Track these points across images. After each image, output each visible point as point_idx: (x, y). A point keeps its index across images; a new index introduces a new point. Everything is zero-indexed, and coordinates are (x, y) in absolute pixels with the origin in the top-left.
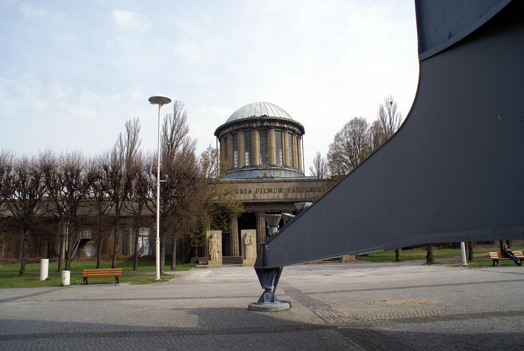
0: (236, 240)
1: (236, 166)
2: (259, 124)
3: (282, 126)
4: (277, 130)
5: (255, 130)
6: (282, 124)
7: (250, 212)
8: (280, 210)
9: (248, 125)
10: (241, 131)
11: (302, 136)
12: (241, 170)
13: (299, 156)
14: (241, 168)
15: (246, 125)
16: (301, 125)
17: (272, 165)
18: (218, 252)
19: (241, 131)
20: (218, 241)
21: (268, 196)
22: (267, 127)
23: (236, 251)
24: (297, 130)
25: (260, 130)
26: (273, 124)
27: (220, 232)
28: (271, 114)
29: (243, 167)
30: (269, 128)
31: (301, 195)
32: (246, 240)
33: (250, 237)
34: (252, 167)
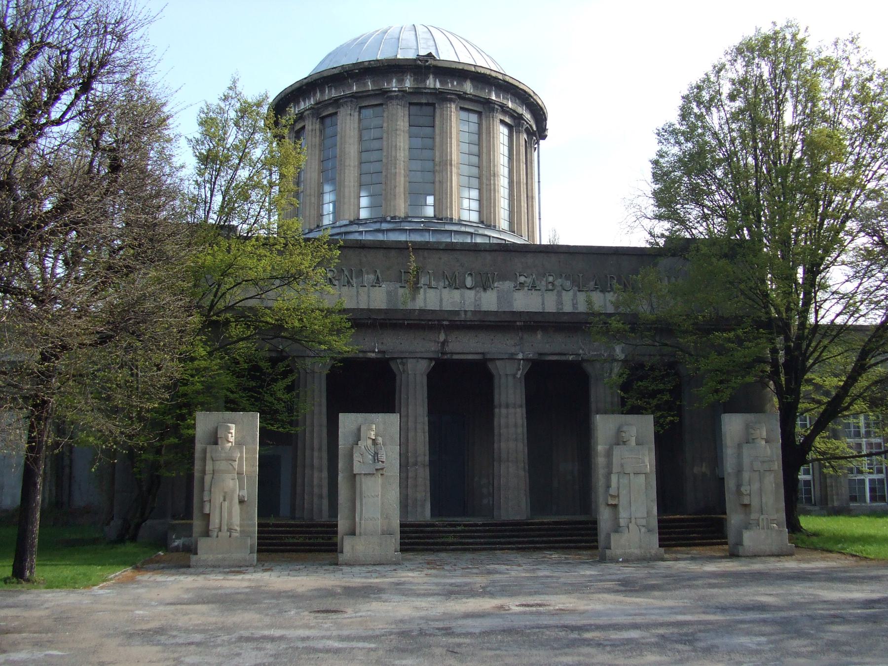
0: (321, 458)
1: (327, 220)
2: (408, 84)
3: (484, 94)
4: (466, 106)
5: (394, 102)
6: (483, 89)
7: (373, 355)
8: (483, 353)
9: (373, 83)
10: (349, 104)
11: (539, 145)
12: (343, 230)
13: (530, 200)
14: (345, 226)
15: (365, 84)
16: (540, 103)
17: (446, 218)
18: (241, 502)
19: (349, 104)
20: (241, 458)
21: (441, 300)
22: (435, 93)
23: (315, 500)
24: (528, 116)
25: (410, 104)
26: (452, 85)
27: (255, 420)
28: (446, 54)
29: (352, 223)
30: (442, 97)
31: (560, 302)
32: (357, 457)
33: (374, 441)
34: (381, 222)
